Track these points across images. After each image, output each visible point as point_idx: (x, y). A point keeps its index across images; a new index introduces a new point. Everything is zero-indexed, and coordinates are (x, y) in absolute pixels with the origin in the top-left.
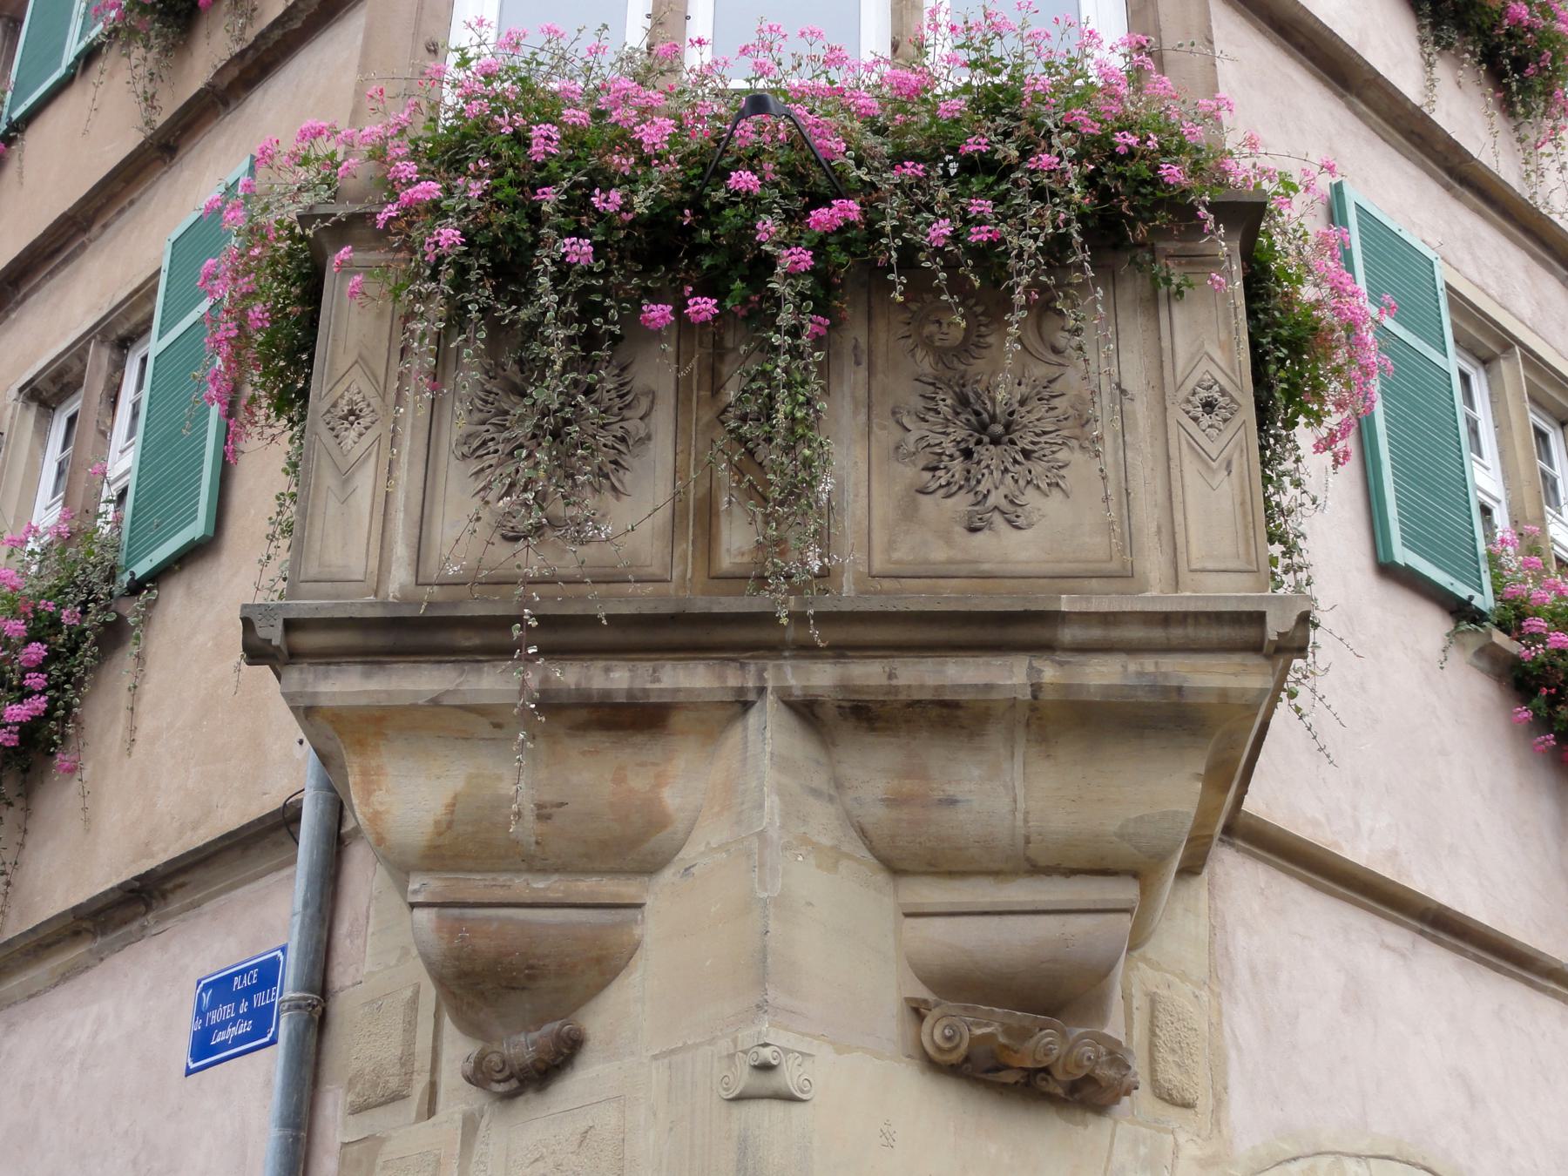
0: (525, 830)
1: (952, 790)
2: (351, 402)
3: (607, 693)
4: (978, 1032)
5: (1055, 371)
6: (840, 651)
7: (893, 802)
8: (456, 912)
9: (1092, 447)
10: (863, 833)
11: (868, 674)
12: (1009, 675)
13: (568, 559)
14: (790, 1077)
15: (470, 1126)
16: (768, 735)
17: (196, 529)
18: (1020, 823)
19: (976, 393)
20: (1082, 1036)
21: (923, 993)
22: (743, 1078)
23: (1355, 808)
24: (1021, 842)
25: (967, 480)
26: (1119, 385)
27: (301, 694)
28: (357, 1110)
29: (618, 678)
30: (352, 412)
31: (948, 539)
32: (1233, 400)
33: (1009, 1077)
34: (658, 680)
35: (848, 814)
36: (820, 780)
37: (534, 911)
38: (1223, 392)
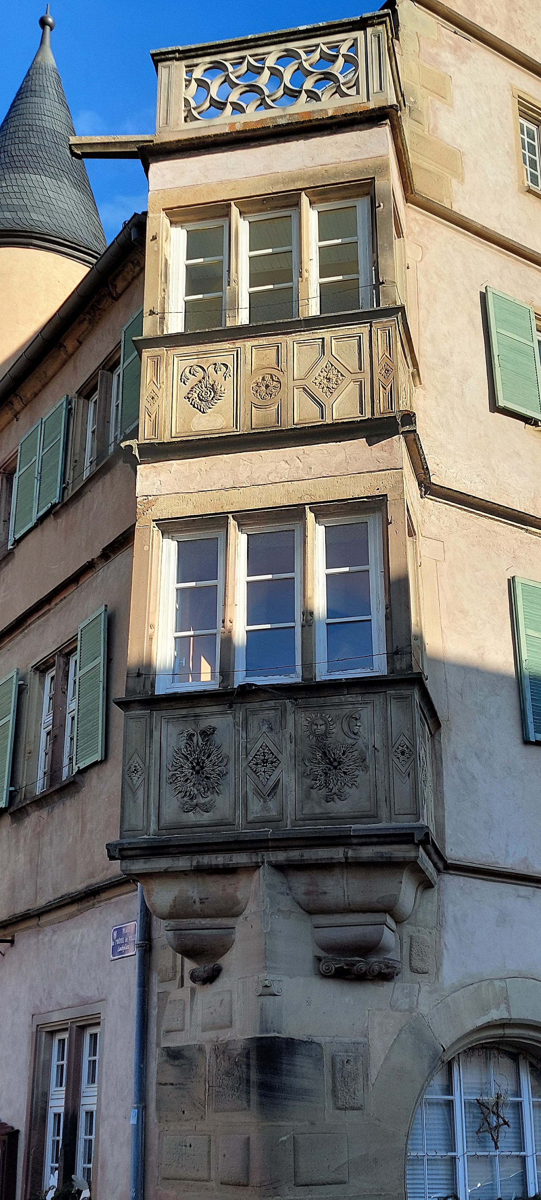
0: (197, 906)
1: (324, 889)
2: (135, 766)
3: (217, 865)
4: (337, 966)
5: (355, 741)
6: (286, 848)
7: (308, 893)
8: (179, 932)
9: (366, 768)
10: (298, 903)
11: (295, 855)
12: (338, 853)
13: (205, 818)
14: (274, 989)
15: (193, 991)
16: (263, 876)
17: (98, 757)
18: (346, 899)
19: (328, 751)
20: (376, 962)
21: (322, 954)
22: (261, 990)
23: (507, 846)
24: (347, 905)
25: (326, 783)
26: (374, 746)
27: (127, 870)
28: (162, 981)
29: (219, 860)
30: (135, 770)
31: (319, 804)
32: (410, 751)
33: (353, 976)
34: (232, 860)
35: (294, 898)
36: (284, 889)
37: (203, 928)
38: (407, 748)
